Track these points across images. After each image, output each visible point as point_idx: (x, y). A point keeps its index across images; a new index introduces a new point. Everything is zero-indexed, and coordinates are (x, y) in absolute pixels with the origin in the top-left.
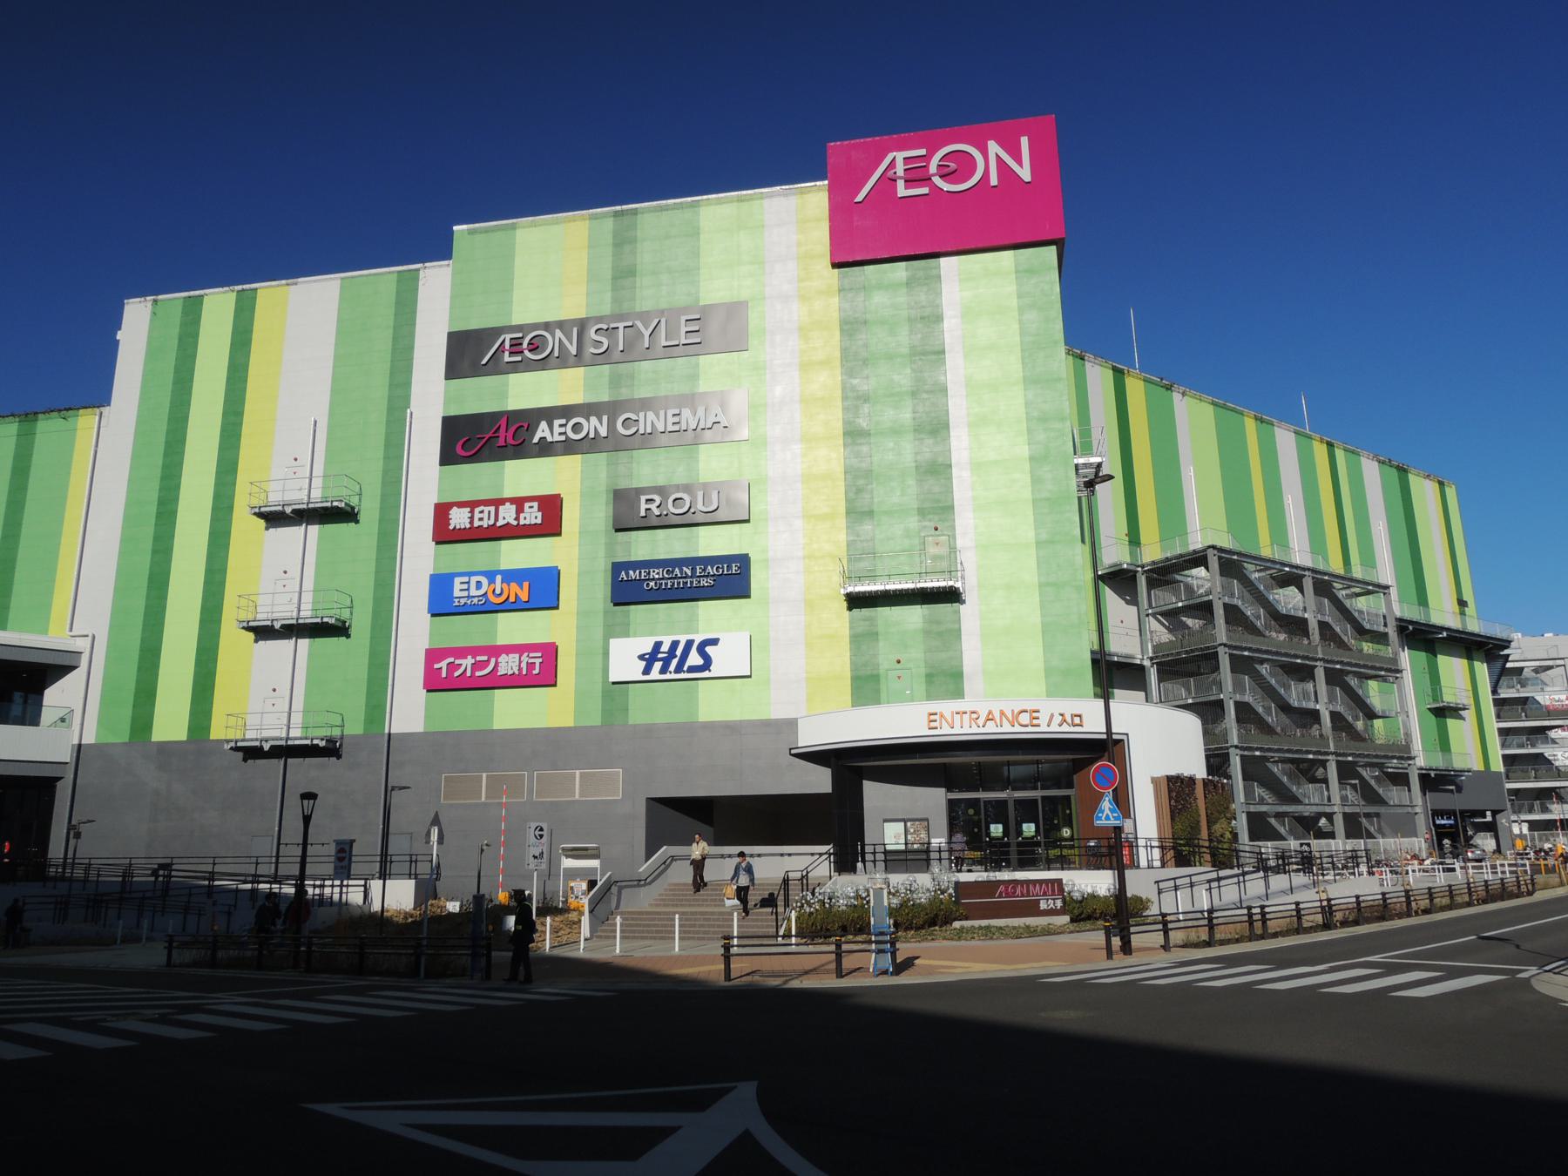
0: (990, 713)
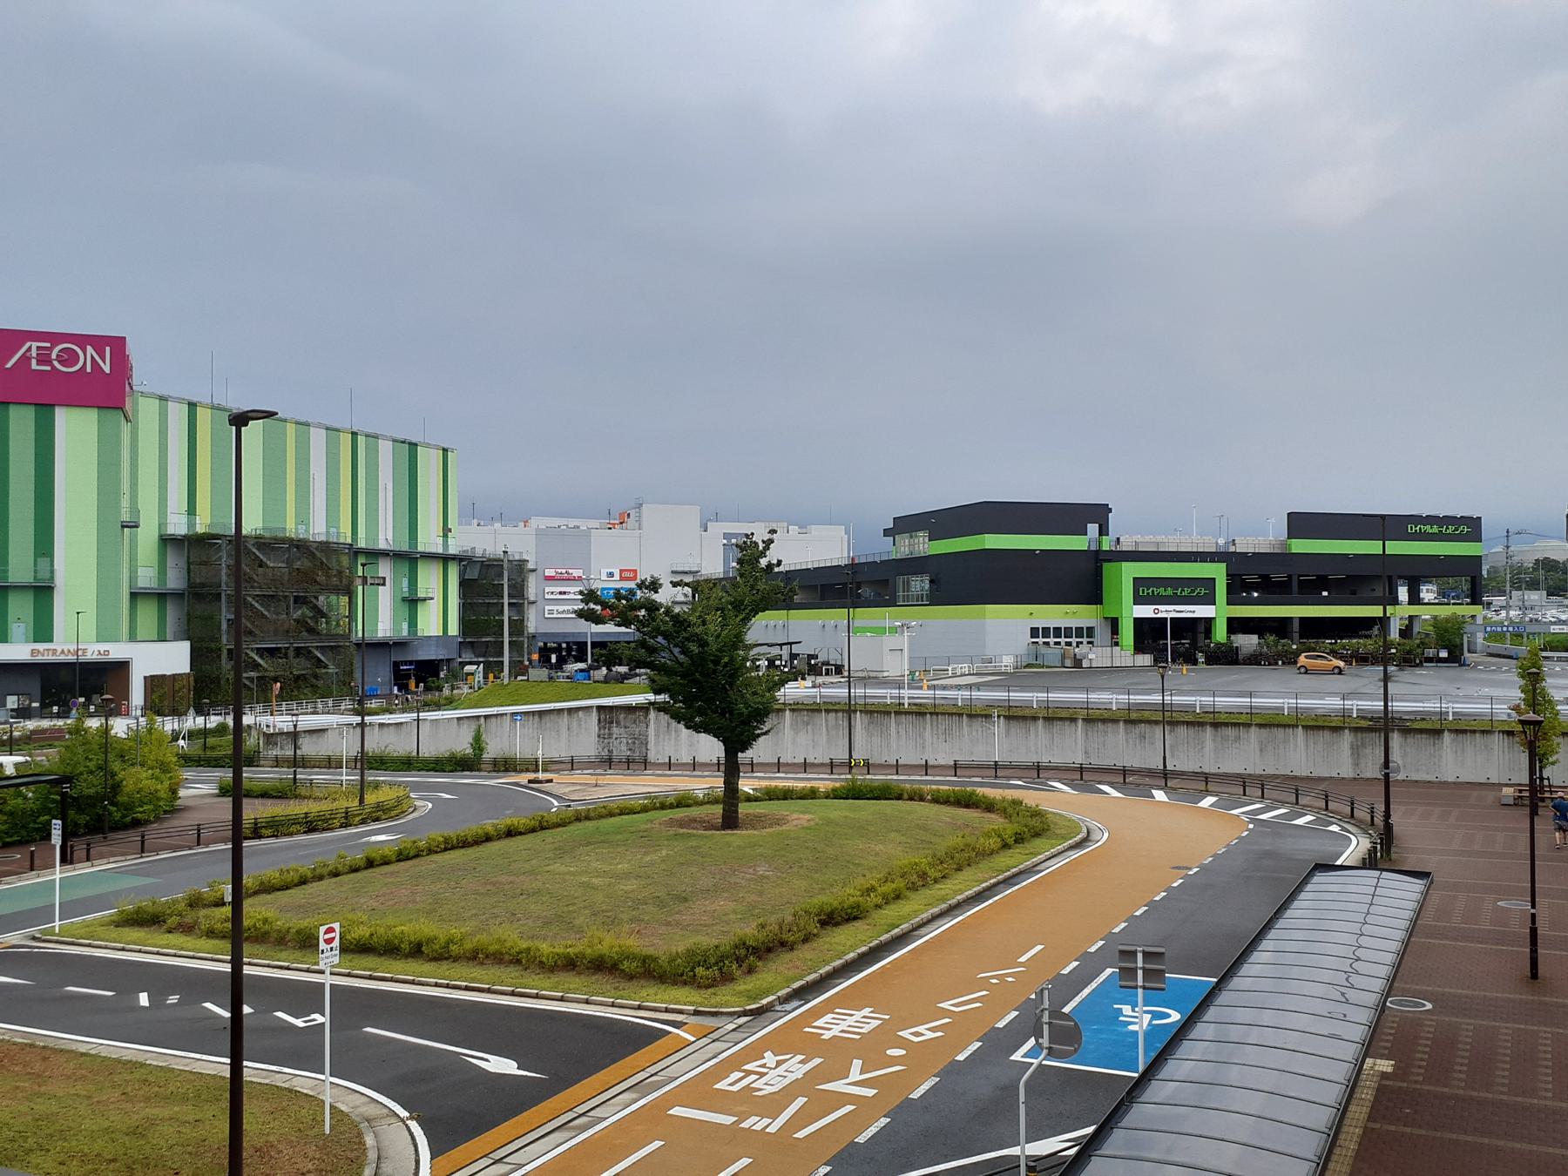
0: (63, 650)
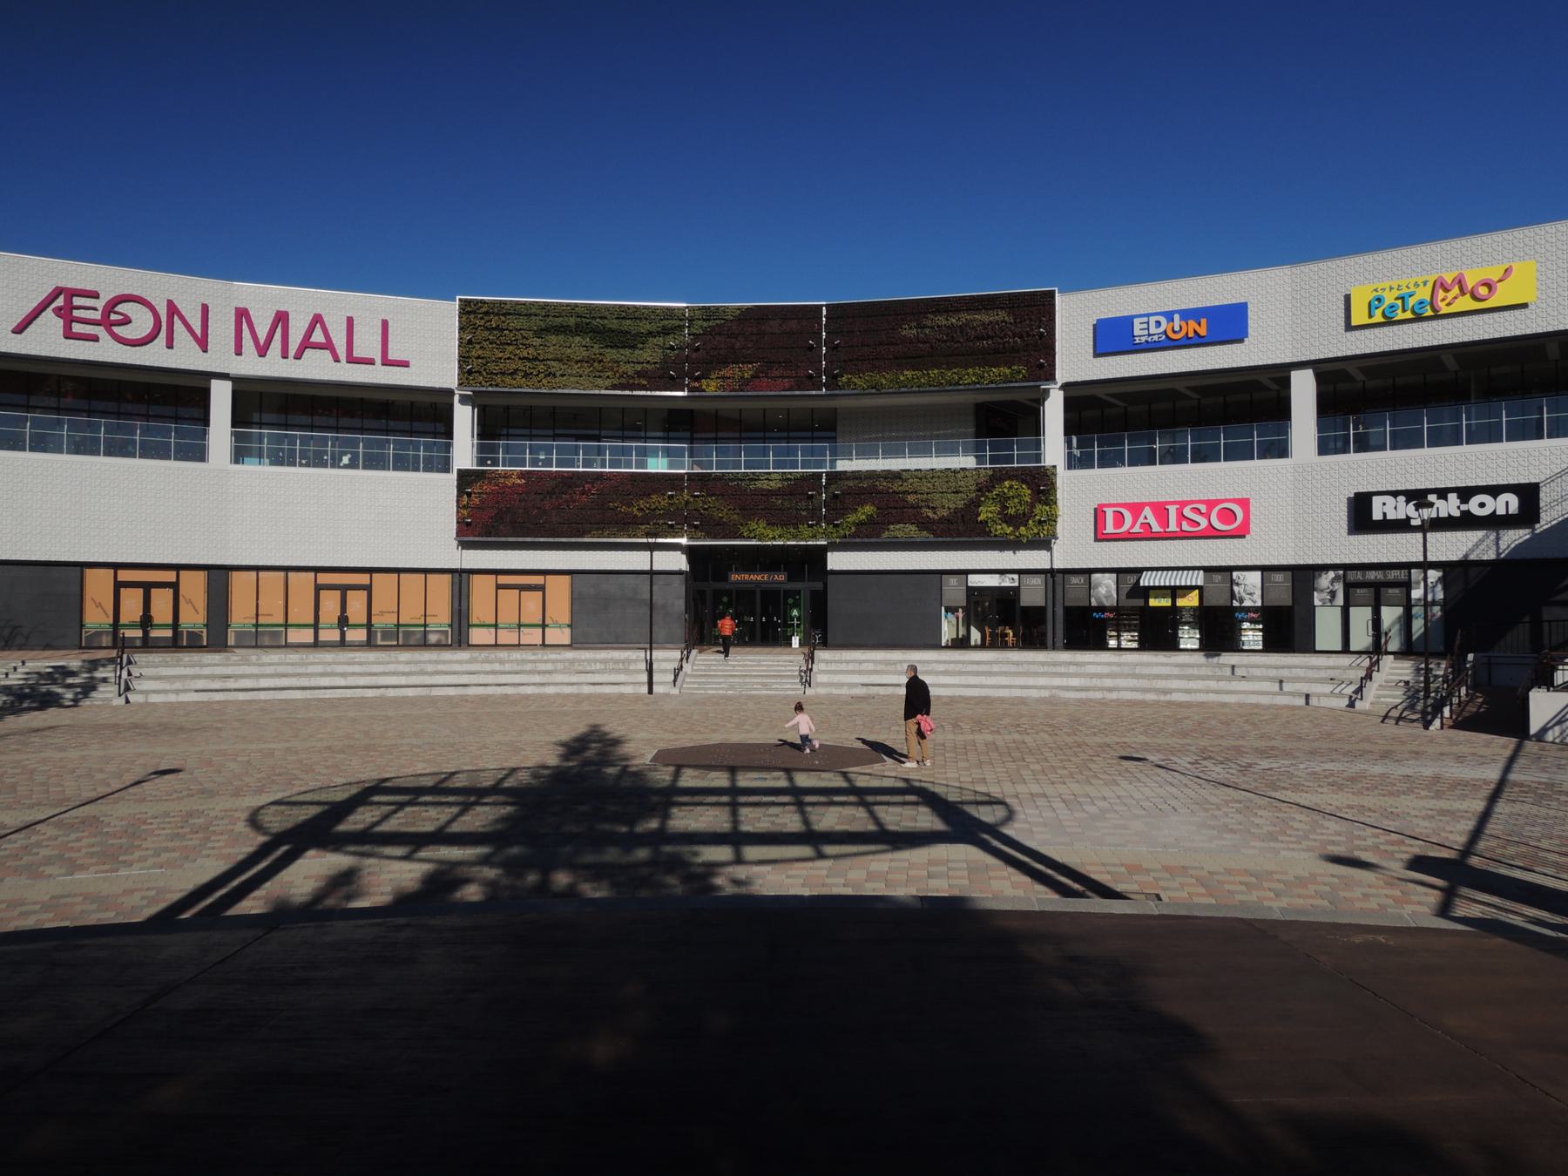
0: (317, 320)
